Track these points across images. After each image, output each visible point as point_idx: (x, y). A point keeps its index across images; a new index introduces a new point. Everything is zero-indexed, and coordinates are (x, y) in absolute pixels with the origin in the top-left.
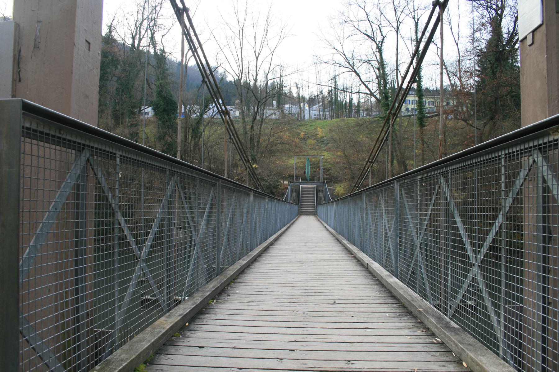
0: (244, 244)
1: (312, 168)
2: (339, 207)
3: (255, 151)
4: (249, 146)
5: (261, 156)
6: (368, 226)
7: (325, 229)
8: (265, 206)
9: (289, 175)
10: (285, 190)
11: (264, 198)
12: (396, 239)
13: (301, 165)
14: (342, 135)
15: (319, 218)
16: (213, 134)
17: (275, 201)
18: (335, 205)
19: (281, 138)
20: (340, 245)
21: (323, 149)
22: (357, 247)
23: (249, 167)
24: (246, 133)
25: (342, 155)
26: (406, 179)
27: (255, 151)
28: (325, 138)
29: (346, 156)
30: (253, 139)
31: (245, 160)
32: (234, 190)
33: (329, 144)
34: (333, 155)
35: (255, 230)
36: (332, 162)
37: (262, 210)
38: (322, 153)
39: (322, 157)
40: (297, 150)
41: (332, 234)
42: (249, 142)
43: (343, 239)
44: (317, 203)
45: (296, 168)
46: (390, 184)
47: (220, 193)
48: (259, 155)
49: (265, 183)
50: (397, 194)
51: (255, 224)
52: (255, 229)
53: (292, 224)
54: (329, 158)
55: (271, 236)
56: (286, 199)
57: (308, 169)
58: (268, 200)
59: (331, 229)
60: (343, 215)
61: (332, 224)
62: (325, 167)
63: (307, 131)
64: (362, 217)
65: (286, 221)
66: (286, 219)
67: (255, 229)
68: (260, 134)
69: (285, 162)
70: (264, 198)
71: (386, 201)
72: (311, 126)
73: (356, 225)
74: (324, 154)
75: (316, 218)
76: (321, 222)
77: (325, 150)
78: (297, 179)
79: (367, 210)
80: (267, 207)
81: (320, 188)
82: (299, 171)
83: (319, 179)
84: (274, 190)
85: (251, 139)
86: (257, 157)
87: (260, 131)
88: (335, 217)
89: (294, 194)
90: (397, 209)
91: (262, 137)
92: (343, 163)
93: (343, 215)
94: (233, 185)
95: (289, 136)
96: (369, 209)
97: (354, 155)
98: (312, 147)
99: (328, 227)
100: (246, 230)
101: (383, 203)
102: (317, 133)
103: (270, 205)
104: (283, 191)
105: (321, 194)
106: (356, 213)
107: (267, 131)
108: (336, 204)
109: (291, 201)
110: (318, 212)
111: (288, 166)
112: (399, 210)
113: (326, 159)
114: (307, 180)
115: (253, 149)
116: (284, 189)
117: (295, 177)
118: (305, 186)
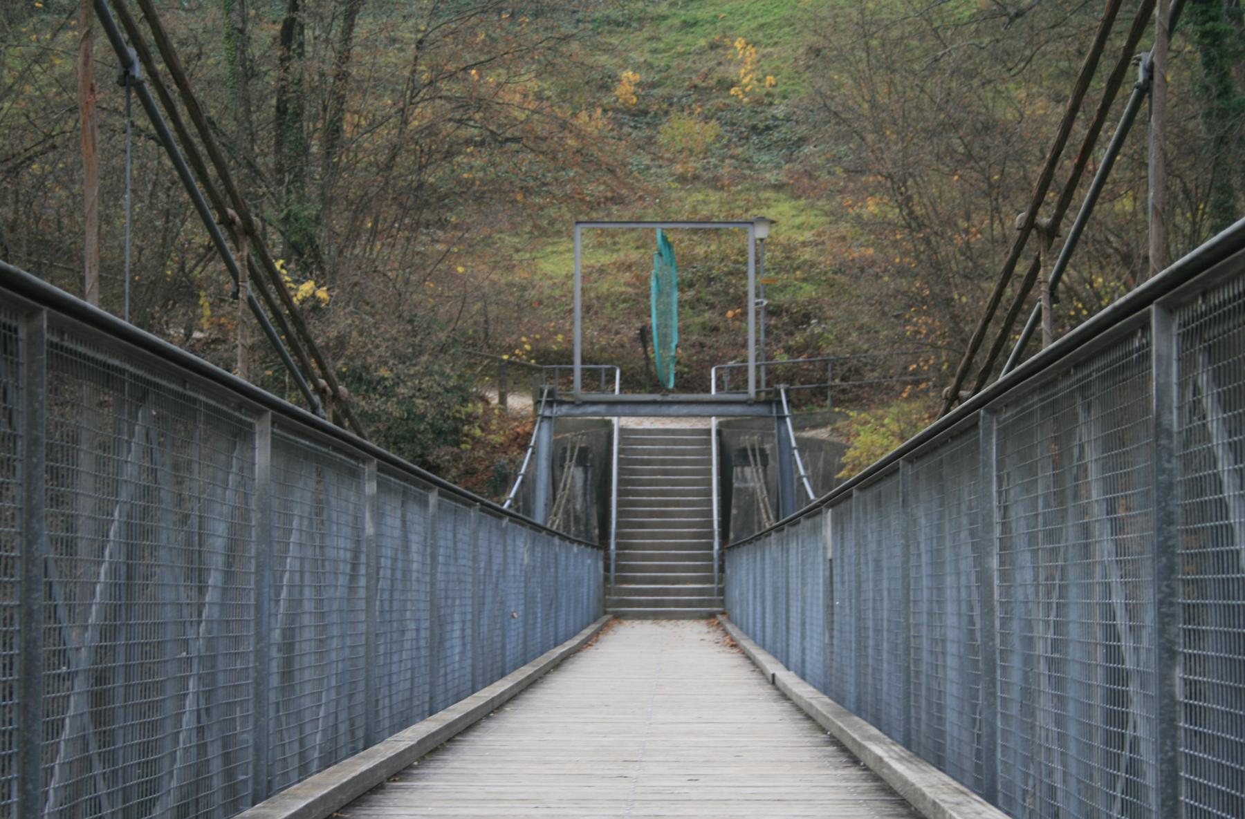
0: (215, 751)
1: (693, 304)
2: (850, 535)
3: (312, 191)
4: (271, 160)
5: (354, 233)
6: (1015, 626)
7: (767, 690)
8: (358, 527)
9: (544, 356)
10: (514, 452)
11: (355, 474)
12: (1164, 678)
13: (619, 284)
14: (891, 83)
15: (735, 632)
16: (22, 78)
17: (433, 498)
18: (828, 532)
19: (482, 104)
20: (853, 772)
21: (771, 177)
22: (957, 774)
23: (251, 267)
24: (247, 72)
25: (893, 214)
26: (1216, 288)
27: (312, 191)
28: (780, 110)
29: (914, 223)
30: (298, 115)
31: (228, 223)
32: (143, 393)
33: (808, 149)
34: (836, 216)
35: (287, 673)
36: (825, 262)
37: (340, 546)
38: (760, 204)
39: (761, 232)
40: (594, 189)
41: (809, 717)
42: (266, 134)
43: (871, 738)
44: (724, 535)
45: (587, 309)
46: (1127, 336)
47: (42, 392)
48: (339, 223)
49: (377, 403)
50: (1163, 391)
51: (289, 634)
52: (288, 663)
53: (558, 665)
54: (808, 236)
55: (405, 723)
56: (525, 499)
57: (663, 314)
58: (381, 485)
59: (804, 691)
60: (877, 582)
61: (815, 660)
62: (782, 298)
63: (661, 61)
64: (983, 578)
65: (513, 645)
66: (516, 628)
67: (288, 663)
68: (342, 76)
69: (510, 268)
70: (355, 474)
71: (1114, 443)
72: (688, 25)
73: (951, 634)
74: (771, 214)
75: (718, 635)
76: (748, 657)
77: (778, 187)
78: (593, 379)
79: (1005, 527)
80: (369, 529)
81: (746, 440)
82: (604, 329)
83: (738, 379)
84: (442, 454)
85: (281, 110)
86: (322, 235)
87: (344, 57)
88: (830, 607)
89: (575, 475)
90: (1170, 486)
91: (354, 102)
92: (901, 272)
93: (877, 582)
94: (129, 357)
95: (539, 97)
96: (1018, 512)
97: (968, 218)
98: (694, 165)
99: (787, 678)
100: (221, 663)
101: (1092, 455)
102: (731, 72)
103: (393, 522)
104: (503, 459)
105: (750, 478)
106: (948, 554)
107: (392, 56)
108: (839, 523)
109: (556, 524)
110: (735, 593)
111: (531, 294)
112: (1179, 491)
113: (789, 249)
114: (657, 385)
115: (299, 177)
116: (504, 448)
117: (578, 365)
118: (647, 424)
